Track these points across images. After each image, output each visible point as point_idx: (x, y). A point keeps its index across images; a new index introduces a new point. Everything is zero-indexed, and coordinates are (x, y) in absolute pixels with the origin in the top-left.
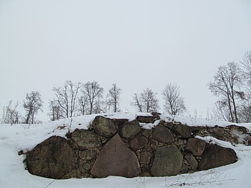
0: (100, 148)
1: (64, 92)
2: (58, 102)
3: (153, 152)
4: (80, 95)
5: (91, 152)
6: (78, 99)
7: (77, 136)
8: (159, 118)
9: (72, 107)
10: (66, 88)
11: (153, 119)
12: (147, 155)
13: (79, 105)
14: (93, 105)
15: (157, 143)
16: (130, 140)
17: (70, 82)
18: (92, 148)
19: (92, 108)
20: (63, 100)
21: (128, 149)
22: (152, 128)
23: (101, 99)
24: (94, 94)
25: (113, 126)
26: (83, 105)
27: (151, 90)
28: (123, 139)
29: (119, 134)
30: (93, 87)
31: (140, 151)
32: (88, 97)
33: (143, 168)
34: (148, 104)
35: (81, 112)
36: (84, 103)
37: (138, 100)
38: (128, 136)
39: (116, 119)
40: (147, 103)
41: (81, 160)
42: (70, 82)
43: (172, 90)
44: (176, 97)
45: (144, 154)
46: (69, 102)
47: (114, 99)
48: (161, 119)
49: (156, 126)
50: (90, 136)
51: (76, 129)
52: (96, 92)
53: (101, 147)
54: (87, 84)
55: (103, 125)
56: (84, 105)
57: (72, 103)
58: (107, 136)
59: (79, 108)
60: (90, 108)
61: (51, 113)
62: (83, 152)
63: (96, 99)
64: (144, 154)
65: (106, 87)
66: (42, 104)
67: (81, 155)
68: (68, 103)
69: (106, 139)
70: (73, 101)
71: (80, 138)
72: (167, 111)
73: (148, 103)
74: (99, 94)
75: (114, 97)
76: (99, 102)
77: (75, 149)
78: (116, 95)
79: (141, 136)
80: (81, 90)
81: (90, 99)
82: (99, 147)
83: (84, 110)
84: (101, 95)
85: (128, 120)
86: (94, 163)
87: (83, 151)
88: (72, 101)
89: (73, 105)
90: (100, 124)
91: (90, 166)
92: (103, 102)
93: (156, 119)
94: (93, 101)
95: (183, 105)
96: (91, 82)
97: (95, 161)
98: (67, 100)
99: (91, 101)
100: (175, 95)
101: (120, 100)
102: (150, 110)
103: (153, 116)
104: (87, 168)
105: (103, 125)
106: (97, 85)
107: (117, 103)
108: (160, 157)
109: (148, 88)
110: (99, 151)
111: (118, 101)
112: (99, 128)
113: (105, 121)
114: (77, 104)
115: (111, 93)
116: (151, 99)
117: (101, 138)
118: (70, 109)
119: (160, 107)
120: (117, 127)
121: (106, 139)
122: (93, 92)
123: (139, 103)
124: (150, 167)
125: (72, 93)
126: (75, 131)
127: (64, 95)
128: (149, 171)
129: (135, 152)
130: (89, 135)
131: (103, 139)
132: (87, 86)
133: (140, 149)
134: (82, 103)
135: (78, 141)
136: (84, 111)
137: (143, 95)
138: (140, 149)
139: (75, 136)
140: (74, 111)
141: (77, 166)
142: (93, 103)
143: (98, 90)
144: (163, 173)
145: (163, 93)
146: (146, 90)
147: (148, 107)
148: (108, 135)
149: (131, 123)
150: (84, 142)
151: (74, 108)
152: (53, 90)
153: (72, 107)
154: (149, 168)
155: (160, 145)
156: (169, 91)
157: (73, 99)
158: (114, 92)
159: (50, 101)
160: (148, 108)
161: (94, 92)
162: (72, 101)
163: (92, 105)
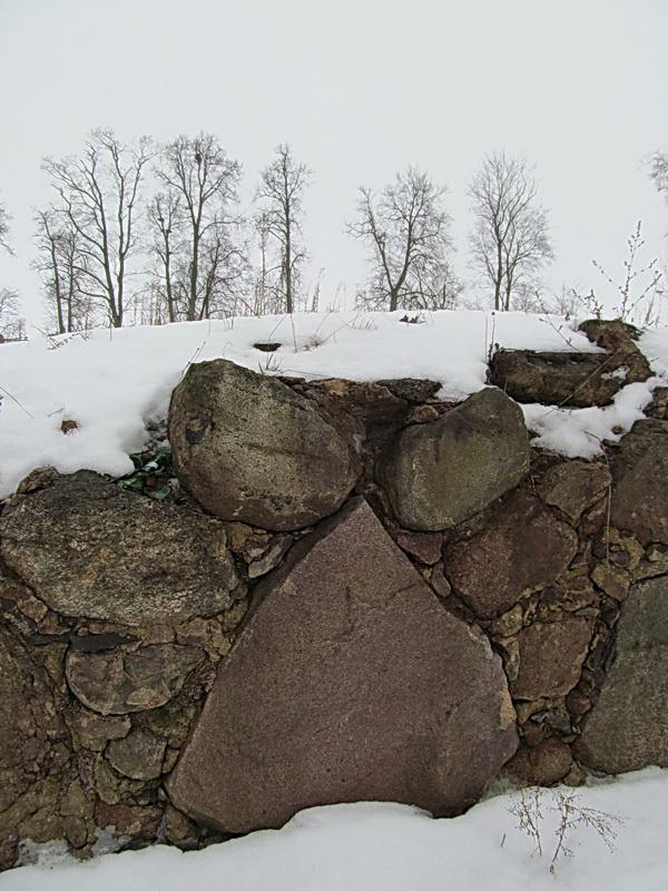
0: (236, 615)
1: (89, 177)
2: (67, 219)
3: (606, 614)
4: (150, 188)
5: (167, 652)
6: (143, 205)
7: (39, 542)
8: (641, 370)
9: (121, 238)
10: (93, 157)
11: (605, 376)
12: (566, 645)
13: (151, 227)
14: (201, 230)
15: (636, 552)
16: (451, 545)
17: (110, 134)
18: (172, 622)
19: (200, 242)
20: (84, 209)
21: (441, 609)
22: (605, 443)
23: (232, 208)
24: (207, 188)
25: (332, 447)
26: (163, 231)
27: (424, 177)
28: (404, 541)
29: (375, 502)
30: (198, 158)
31: (519, 617)
32: (183, 196)
33: (536, 723)
34: (410, 230)
35: (156, 255)
36: (166, 223)
37: (374, 213)
38: (443, 519)
39: (352, 384)
40: (407, 226)
41: (84, 722)
42: (110, 134)
43: (505, 175)
44: (518, 206)
45: (544, 638)
46: (109, 218)
47: (280, 207)
48: (654, 374)
49: (628, 428)
50: (149, 537)
51: (28, 480)
52: (212, 178)
53: (243, 606)
54: (176, 145)
55: (251, 446)
56: (169, 231)
57: (121, 220)
58: (280, 526)
59: (152, 241)
60: (192, 243)
61: (45, 259)
62: (95, 659)
63: (213, 207)
64: (544, 638)
65: (251, 156)
66: (7, 223)
67: (83, 686)
68: (106, 221)
69: (277, 550)
70: (125, 212)
71: (68, 555)
72: (481, 259)
73: (410, 226)
74: (223, 186)
75: (281, 200)
76: (226, 220)
77: (38, 639)
78: (289, 191)
79: (536, 515)
80: (154, 168)
81: (191, 208)
82: (222, 612)
83: (168, 249)
84: (233, 189)
85: (438, 386)
86: (190, 729)
87: (101, 652)
88: (121, 212)
89: (125, 230)
90: (227, 439)
91: (157, 757)
92: (239, 221)
93: (621, 373)
94: (203, 213)
95: (543, 239)
96: (192, 139)
97: (197, 715)
98: (101, 210)
99: (193, 216)
100: (516, 199)
101: (305, 213)
102: (416, 253)
103: (593, 348)
104: (143, 761)
105: (251, 446)
106: (214, 148)
107: (292, 225)
108: (649, 647)
109: (414, 166)
110: (224, 646)
111: (297, 217)
112: (222, 467)
113: (265, 415)
114: (143, 225)
115: (270, 182)
116: (422, 213)
117: (239, 542)
118: (113, 246)
119: (455, 243)
120: (357, 439)
121: (277, 550)
122: (202, 178)
123: (377, 226)
124: (577, 717)
125: (120, 182)
126: (29, 492)
127: (87, 188)
128: (571, 739)
129: (486, 631)
130: (142, 527)
131: (255, 552)
132: (177, 153)
133: (524, 604)
134: (162, 220)
135: (49, 582)
136: (168, 254)
137: (392, 195)
138: (524, 604)
139: (28, 542)
140: (129, 251)
141: (61, 755)
142: (201, 223)
143: (220, 169)
144: (657, 742)
145: (470, 186)
146: (404, 175)
147: (411, 240)
148: (290, 519)
149: (462, 419)
150: (103, 585)
151: (131, 243)
152: (43, 168)
153: (121, 238)
154: (572, 723)
155: (652, 570)
156: (496, 183)
157: (125, 206)
158: (283, 180)
159: (37, 215)
160: (409, 248)
161: (205, 180)
162: (121, 212)
163: (200, 232)
